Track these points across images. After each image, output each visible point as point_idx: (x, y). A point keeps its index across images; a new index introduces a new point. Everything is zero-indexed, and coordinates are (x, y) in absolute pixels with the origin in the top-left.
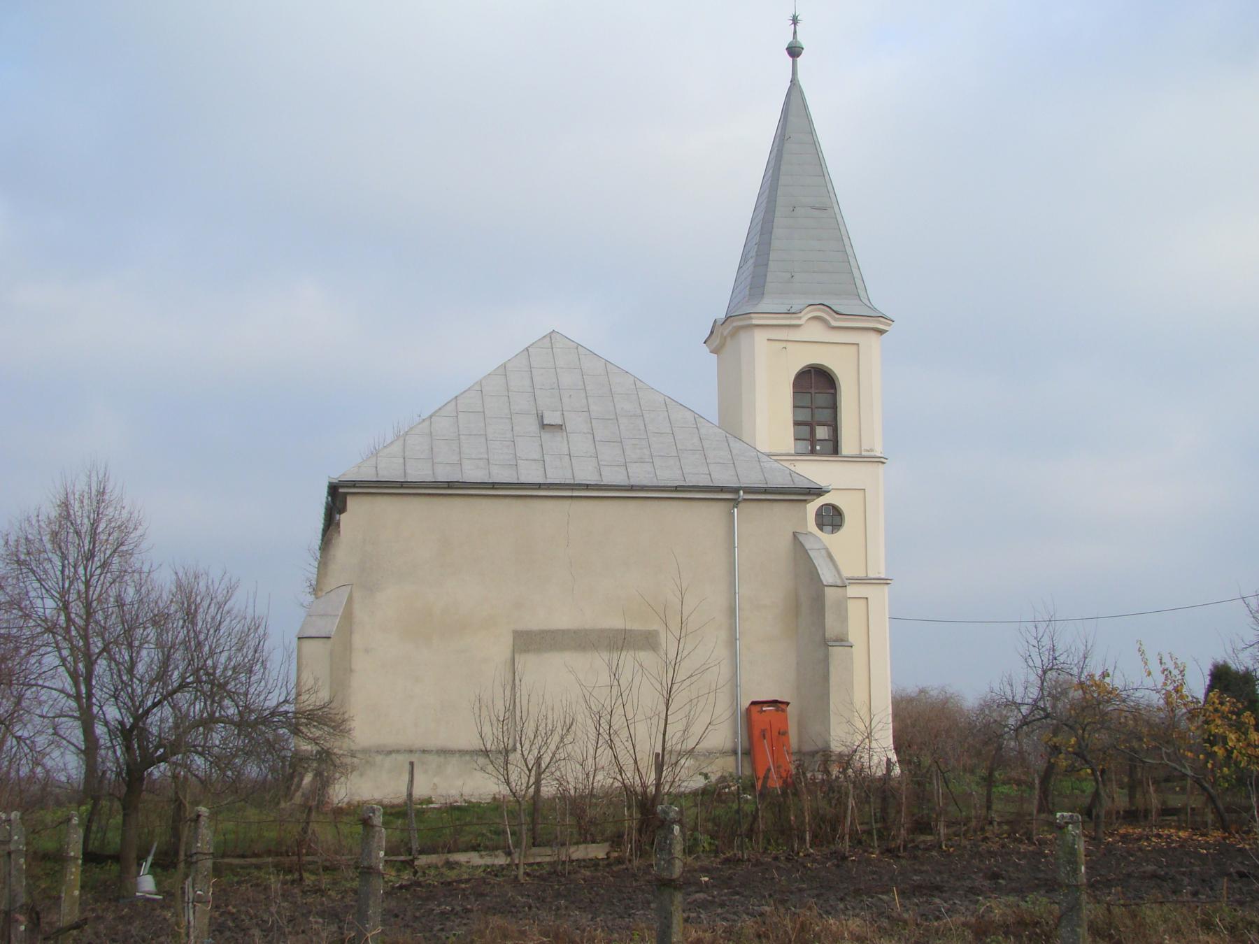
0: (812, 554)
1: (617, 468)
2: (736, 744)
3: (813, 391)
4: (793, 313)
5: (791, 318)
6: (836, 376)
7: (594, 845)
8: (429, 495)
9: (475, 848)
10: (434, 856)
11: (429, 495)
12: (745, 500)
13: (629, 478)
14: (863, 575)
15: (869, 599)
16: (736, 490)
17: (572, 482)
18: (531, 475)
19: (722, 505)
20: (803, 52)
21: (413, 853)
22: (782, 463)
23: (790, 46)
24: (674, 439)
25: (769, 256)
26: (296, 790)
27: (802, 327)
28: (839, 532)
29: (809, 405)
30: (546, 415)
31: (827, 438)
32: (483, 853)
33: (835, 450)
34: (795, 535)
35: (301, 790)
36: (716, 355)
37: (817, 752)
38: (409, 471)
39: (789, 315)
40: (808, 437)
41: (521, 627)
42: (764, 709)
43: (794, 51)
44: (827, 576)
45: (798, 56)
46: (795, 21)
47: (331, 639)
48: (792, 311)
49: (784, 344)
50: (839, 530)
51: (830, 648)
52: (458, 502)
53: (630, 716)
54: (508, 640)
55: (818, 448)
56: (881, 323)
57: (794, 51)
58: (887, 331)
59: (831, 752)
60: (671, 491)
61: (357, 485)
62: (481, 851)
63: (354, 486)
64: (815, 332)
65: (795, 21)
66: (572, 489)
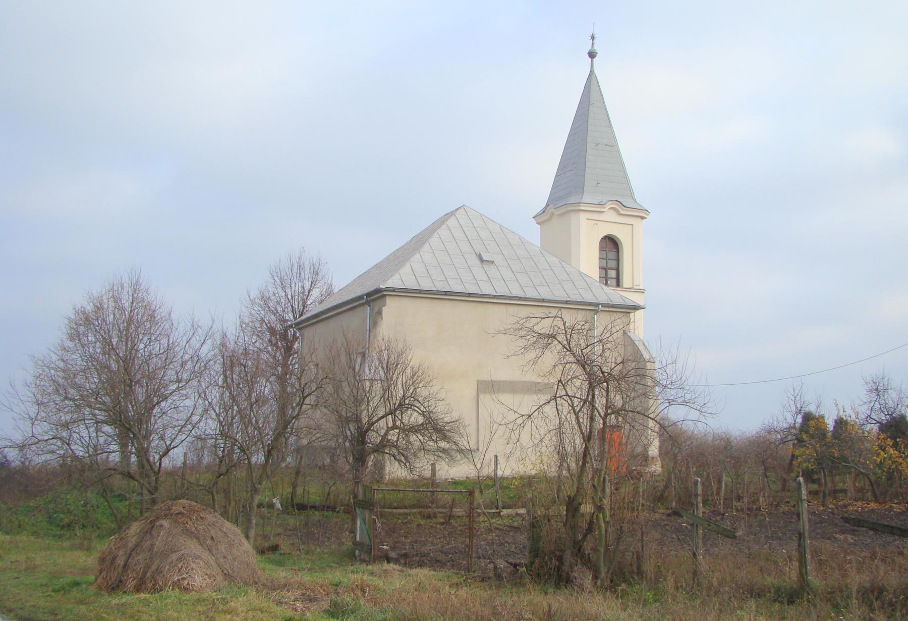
3: (607, 250)
6: (619, 240)
10: (510, 510)
12: (601, 311)
16: (597, 305)
20: (598, 55)
22: (618, 292)
46: (593, 38)
52: (447, 303)
57: (592, 55)
63: (394, 291)
64: (610, 216)
65: (593, 38)
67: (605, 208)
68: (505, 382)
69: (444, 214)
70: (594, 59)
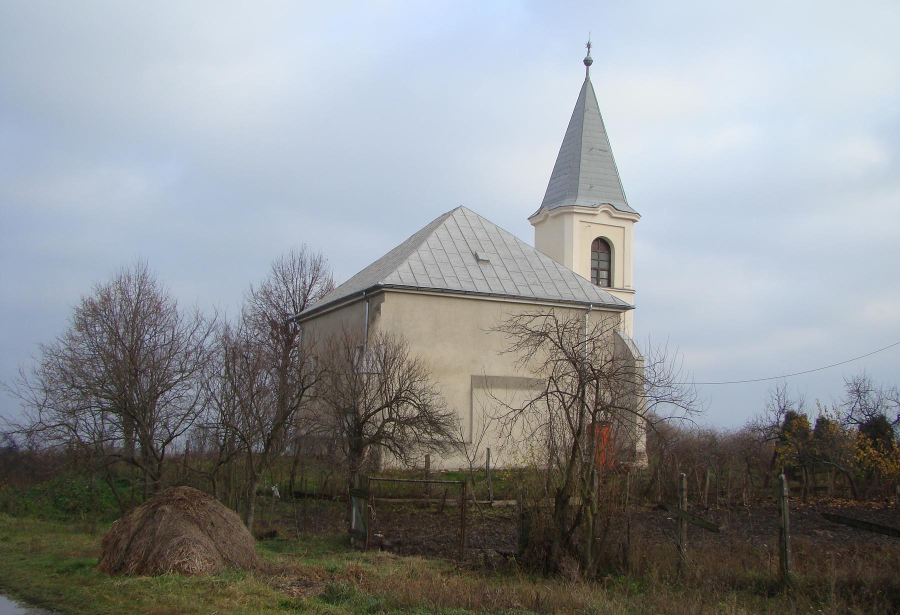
3: (599, 251)
5: (594, 210)
8: (409, 293)
10: (501, 501)
11: (409, 293)
12: (593, 310)
16: (589, 304)
24: (547, 272)
29: (597, 259)
41: (475, 374)
45: (590, 65)
46: (589, 46)
52: (444, 301)
54: (468, 381)
55: (600, 283)
57: (588, 63)
58: (637, 221)
60: (555, 302)
63: (392, 288)
64: (603, 218)
65: (589, 46)
68: (497, 377)
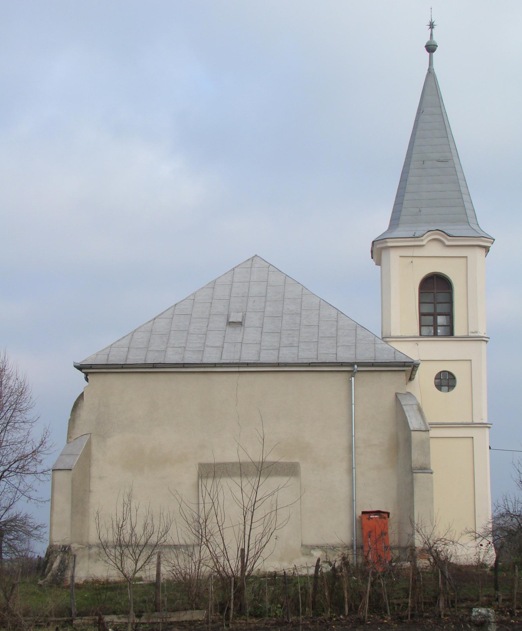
0: (405, 408)
1: (272, 351)
2: (352, 541)
4: (417, 237)
5: (415, 241)
7: (197, 611)
9: (115, 613)
12: (358, 371)
13: (278, 358)
14: (470, 421)
15: (474, 438)
16: (352, 365)
17: (238, 361)
18: (211, 357)
19: (345, 376)
21: (72, 616)
23: (427, 45)
25: (404, 197)
26: (49, 572)
27: (424, 247)
28: (453, 390)
29: (433, 301)
30: (232, 314)
31: (445, 324)
32: (120, 616)
33: (451, 333)
34: (396, 395)
35: (51, 572)
36: (380, 266)
37: (408, 548)
38: (130, 357)
39: (413, 239)
40: (432, 324)
41: (204, 461)
42: (371, 517)
43: (431, 48)
44: (414, 423)
45: (434, 52)
46: (432, 26)
47: (72, 470)
48: (416, 235)
49: (410, 260)
50: (453, 389)
51: (414, 474)
53: (220, 524)
54: (194, 471)
56: (482, 241)
57: (431, 48)
59: (415, 547)
61: (92, 367)
62: (119, 614)
64: (435, 249)
65: (432, 26)
66: (239, 367)
67: (422, 240)
69: (490, 250)
70: (434, 54)
